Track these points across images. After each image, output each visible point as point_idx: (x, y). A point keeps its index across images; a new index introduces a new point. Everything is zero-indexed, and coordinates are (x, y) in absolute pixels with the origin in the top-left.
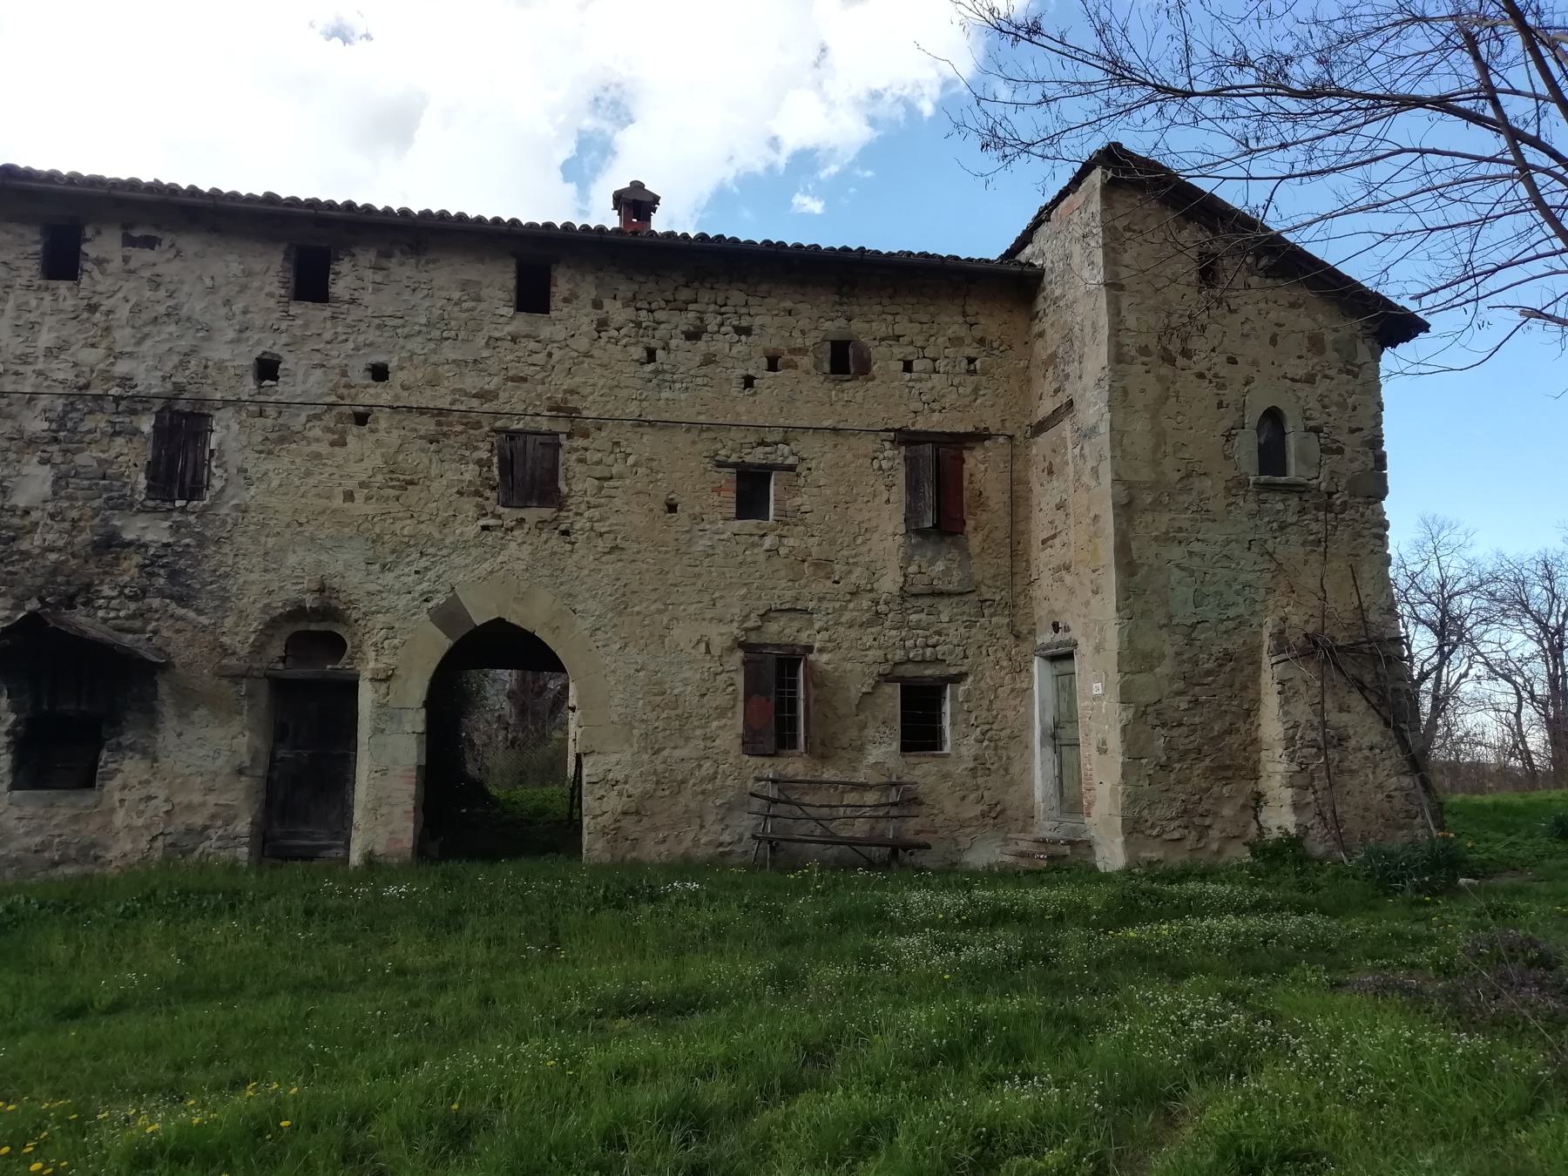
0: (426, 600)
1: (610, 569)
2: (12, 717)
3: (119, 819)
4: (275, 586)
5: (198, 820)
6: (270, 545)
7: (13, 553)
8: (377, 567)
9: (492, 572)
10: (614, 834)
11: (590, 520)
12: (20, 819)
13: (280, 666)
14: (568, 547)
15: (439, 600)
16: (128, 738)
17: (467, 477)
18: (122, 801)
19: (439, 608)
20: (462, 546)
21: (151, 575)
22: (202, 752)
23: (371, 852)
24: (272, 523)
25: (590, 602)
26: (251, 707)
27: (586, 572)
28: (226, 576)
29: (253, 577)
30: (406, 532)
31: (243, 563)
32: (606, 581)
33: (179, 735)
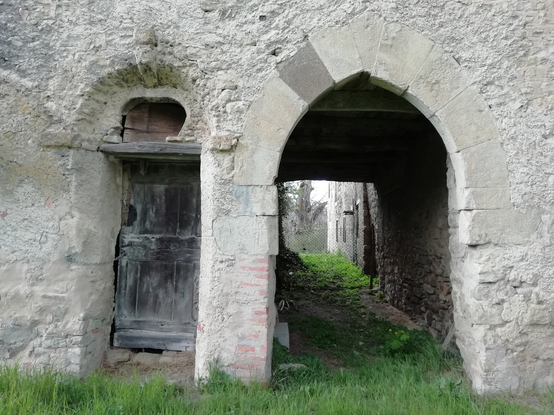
0: (274, 53)
4: (101, 40)
5: (27, 314)
8: (215, 15)
9: (352, 14)
10: (520, 351)
13: (116, 138)
15: (288, 51)
23: (217, 361)
26: (79, 185)
27: (472, 9)
28: (49, 30)
29: (79, 30)
31: (66, 15)
32: (498, 19)
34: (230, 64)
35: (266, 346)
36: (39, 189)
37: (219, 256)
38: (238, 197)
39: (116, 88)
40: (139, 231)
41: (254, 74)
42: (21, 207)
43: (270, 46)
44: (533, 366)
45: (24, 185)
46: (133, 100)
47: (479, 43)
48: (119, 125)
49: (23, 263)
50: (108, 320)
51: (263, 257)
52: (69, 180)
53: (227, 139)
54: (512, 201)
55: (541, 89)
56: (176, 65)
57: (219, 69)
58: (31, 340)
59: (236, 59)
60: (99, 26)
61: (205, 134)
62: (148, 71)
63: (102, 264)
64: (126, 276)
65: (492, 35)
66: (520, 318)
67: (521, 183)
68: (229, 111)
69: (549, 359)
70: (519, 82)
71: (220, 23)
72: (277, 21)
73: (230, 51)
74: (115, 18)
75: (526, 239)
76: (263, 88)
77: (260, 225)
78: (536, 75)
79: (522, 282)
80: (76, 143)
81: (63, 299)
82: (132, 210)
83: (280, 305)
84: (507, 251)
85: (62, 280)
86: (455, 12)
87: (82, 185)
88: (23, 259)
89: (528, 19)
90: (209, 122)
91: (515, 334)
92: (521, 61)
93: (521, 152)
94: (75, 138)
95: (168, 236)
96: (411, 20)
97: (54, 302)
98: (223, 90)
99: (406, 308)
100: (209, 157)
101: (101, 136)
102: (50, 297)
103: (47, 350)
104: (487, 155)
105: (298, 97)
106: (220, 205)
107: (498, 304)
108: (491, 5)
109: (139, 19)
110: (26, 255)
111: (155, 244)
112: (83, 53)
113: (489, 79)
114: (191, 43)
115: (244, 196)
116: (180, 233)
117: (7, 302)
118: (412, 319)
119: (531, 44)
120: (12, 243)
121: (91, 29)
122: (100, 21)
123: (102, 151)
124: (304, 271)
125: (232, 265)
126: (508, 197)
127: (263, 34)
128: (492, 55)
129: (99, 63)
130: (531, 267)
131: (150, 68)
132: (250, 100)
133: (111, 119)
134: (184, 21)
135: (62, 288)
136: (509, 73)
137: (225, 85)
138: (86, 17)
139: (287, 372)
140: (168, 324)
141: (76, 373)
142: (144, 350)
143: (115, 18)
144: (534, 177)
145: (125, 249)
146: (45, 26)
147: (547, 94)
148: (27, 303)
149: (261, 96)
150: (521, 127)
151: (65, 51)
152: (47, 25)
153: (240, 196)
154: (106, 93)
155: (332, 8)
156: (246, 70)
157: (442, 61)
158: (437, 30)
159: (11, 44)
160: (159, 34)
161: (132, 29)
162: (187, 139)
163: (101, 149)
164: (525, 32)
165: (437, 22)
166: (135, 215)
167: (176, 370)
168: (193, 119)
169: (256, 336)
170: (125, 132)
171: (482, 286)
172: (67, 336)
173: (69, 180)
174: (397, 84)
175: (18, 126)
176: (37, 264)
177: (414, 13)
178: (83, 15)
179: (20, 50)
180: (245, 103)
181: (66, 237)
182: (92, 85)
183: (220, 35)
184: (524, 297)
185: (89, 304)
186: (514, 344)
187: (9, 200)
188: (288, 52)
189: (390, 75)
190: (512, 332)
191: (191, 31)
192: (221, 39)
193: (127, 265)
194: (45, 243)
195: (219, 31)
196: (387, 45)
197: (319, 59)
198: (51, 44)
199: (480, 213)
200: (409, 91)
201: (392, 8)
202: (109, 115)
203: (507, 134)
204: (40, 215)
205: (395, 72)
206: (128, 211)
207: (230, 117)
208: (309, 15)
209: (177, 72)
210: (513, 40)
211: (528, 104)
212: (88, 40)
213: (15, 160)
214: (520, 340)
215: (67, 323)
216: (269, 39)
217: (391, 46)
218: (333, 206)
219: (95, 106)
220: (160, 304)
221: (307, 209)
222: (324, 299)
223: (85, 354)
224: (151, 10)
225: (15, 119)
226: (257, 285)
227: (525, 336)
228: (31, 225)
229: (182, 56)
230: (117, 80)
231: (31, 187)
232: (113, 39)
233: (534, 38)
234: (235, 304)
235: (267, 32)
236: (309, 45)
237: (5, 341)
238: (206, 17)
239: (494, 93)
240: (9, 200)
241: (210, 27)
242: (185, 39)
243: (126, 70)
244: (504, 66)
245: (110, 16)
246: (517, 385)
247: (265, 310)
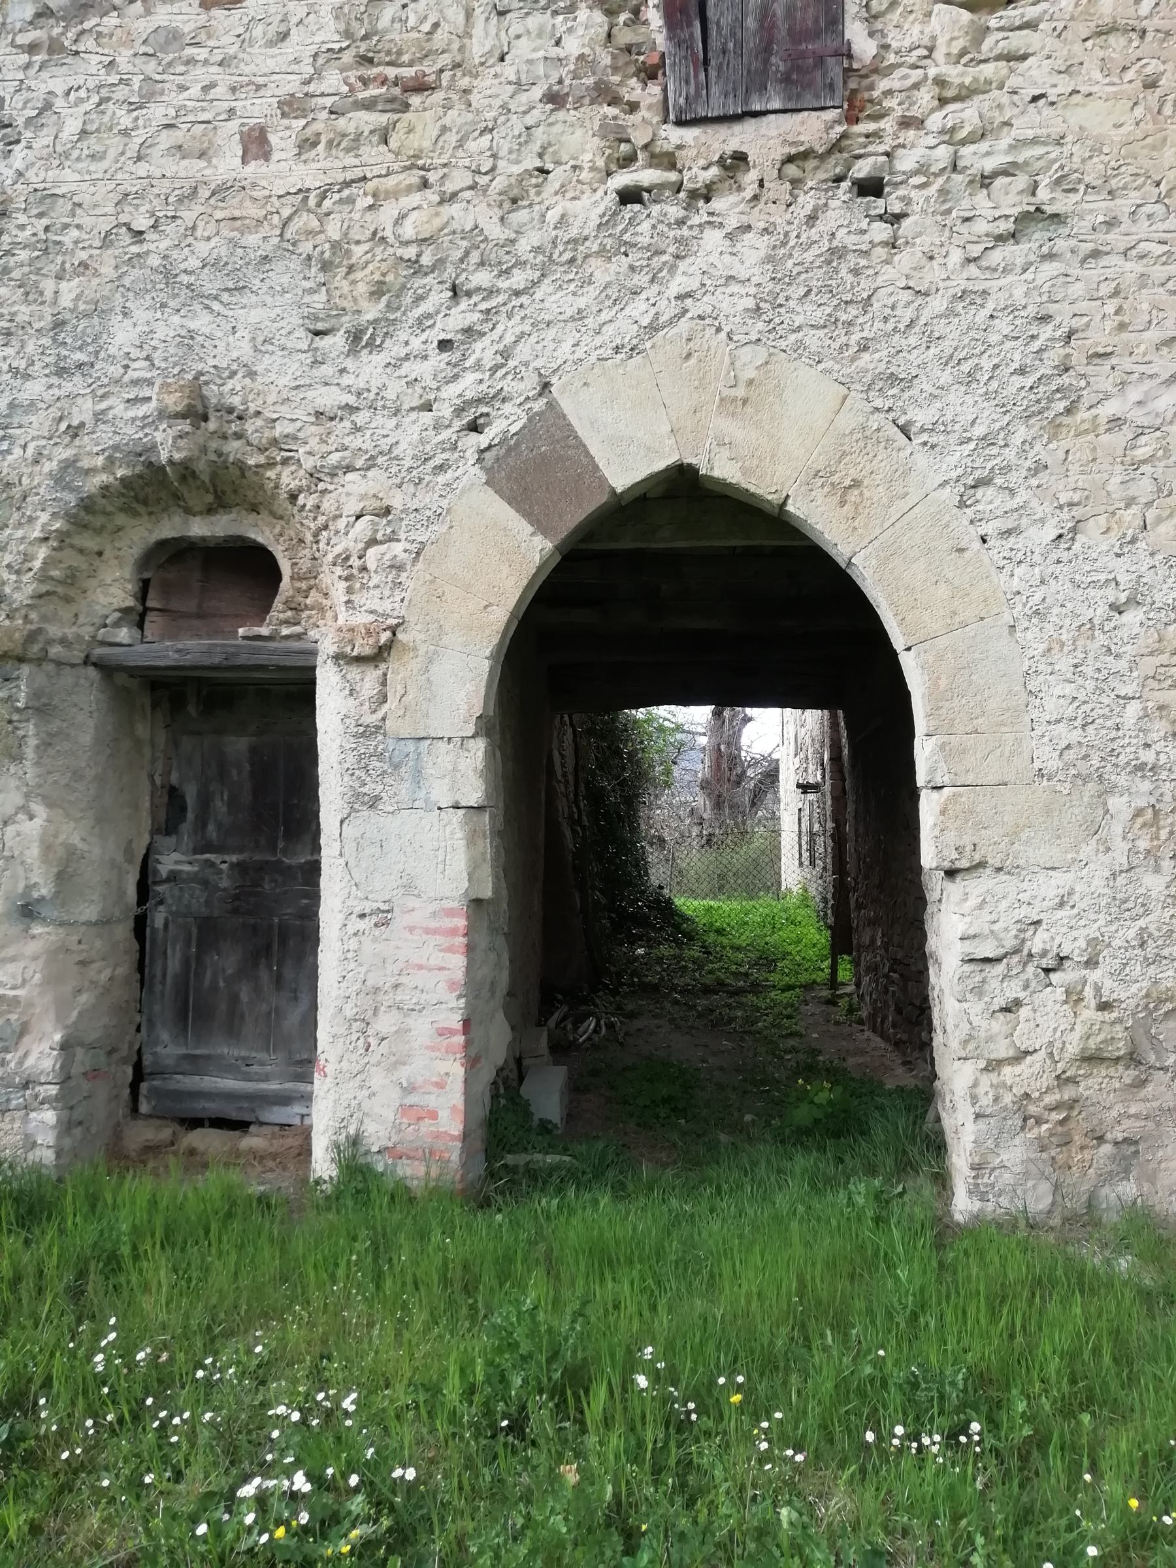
0: (474, 427)
1: (1016, 288)
4: (82, 412)
6: (66, 301)
8: (337, 342)
9: (653, 328)
10: (1059, 1123)
11: (949, 134)
13: (124, 634)
14: (881, 232)
15: (506, 422)
17: (573, 47)
19: (509, 446)
20: (565, 257)
23: (355, 1141)
25: (955, 396)
26: (45, 745)
27: (938, 304)
29: (34, 389)
30: (408, 230)
32: (1003, 326)
34: (372, 458)
35: (461, 1107)
37: (356, 903)
38: (396, 767)
39: (121, 519)
40: (191, 846)
41: (427, 478)
43: (463, 410)
44: (1087, 1156)
46: (162, 544)
47: (956, 387)
48: (130, 602)
50: (124, 1051)
51: (456, 905)
52: (21, 733)
53: (369, 633)
54: (1037, 765)
55: (1108, 493)
56: (251, 462)
57: (349, 469)
59: (385, 444)
60: (77, 379)
61: (328, 619)
62: (190, 480)
63: (104, 922)
64: (165, 953)
65: (987, 364)
66: (1058, 1044)
67: (1058, 721)
68: (372, 566)
69: (1127, 1141)
70: (1053, 478)
71: (349, 360)
72: (478, 351)
73: (373, 425)
74: (111, 359)
75: (1069, 856)
76: (448, 510)
77: (448, 830)
78: (1094, 460)
79: (1062, 959)
80: (36, 648)
81: (16, 1001)
82: (174, 795)
83: (581, 1030)
84: (1025, 885)
85: (13, 959)
86: (897, 313)
87: (50, 744)
89: (1077, 323)
90: (333, 592)
91: (1047, 1080)
92: (1059, 425)
93: (1057, 647)
94: (32, 637)
95: (257, 857)
96: (793, 337)
98: (358, 517)
99: (895, 1034)
100: (331, 674)
101: (91, 629)
104: (977, 656)
105: (531, 529)
106: (356, 784)
107: (1006, 1010)
108: (985, 293)
109: (166, 360)
111: (229, 877)
112: (44, 442)
113: (979, 472)
114: (284, 410)
115: (411, 763)
116: (285, 851)
118: (905, 1063)
119: (1083, 383)
122: (80, 366)
123: (95, 665)
124: (679, 945)
125: (386, 923)
126: (1026, 756)
127: (447, 383)
128: (987, 413)
129: (79, 464)
130: (1083, 922)
131: (194, 472)
132: (420, 539)
133: (112, 590)
134: (267, 359)
135: (14, 976)
136: (1030, 455)
137: (361, 505)
138: (48, 360)
139: (521, 1170)
140: (262, 1064)
141: (46, 1166)
142: (207, 1123)
143: (111, 359)
144: (1090, 706)
145: (160, 888)
147: (1122, 505)
149: (444, 528)
150: (1059, 588)
153: (401, 762)
154: (99, 531)
155: (605, 316)
156: (410, 470)
157: (868, 433)
158: (853, 360)
160: (212, 391)
161: (150, 383)
162: (285, 631)
163: (93, 659)
164: (1068, 356)
165: (854, 338)
166: (183, 809)
167: (271, 1164)
168: (298, 584)
169: (440, 1085)
170: (148, 619)
171: (968, 968)
172: (26, 1085)
173: (21, 733)
174: (760, 492)
177: (799, 320)
180: (408, 546)
182: (67, 514)
183: (348, 389)
184: (1068, 993)
185: (75, 1013)
186: (1042, 1104)
188: (506, 423)
189: (744, 471)
190: (1038, 1076)
191: (284, 381)
192: (351, 400)
193: (166, 926)
195: (347, 380)
196: (735, 400)
197: (576, 437)
199: (961, 795)
200: (790, 508)
201: (747, 310)
202: (109, 581)
203: (1024, 605)
205: (755, 463)
206: (166, 799)
207: (375, 580)
208: (551, 333)
209: (255, 478)
210: (1038, 375)
211: (1074, 530)
212: (54, 412)
214: (1058, 1097)
215: (26, 1055)
216: (460, 395)
217: (745, 401)
218: (792, 770)
219: (77, 561)
220: (242, 1017)
221: (733, 778)
222: (700, 1016)
223: (66, 1127)
224: (192, 338)
226: (441, 969)
227: (1071, 1086)
229: (264, 441)
230: (123, 500)
232: (111, 408)
233: (1091, 367)
234: (394, 1011)
235: (456, 377)
236: (552, 405)
238: (316, 349)
239: (991, 507)
241: (327, 370)
242: (270, 400)
243: (140, 476)
244: (1017, 440)
245: (102, 355)
246: (1049, 1200)
247: (459, 1026)
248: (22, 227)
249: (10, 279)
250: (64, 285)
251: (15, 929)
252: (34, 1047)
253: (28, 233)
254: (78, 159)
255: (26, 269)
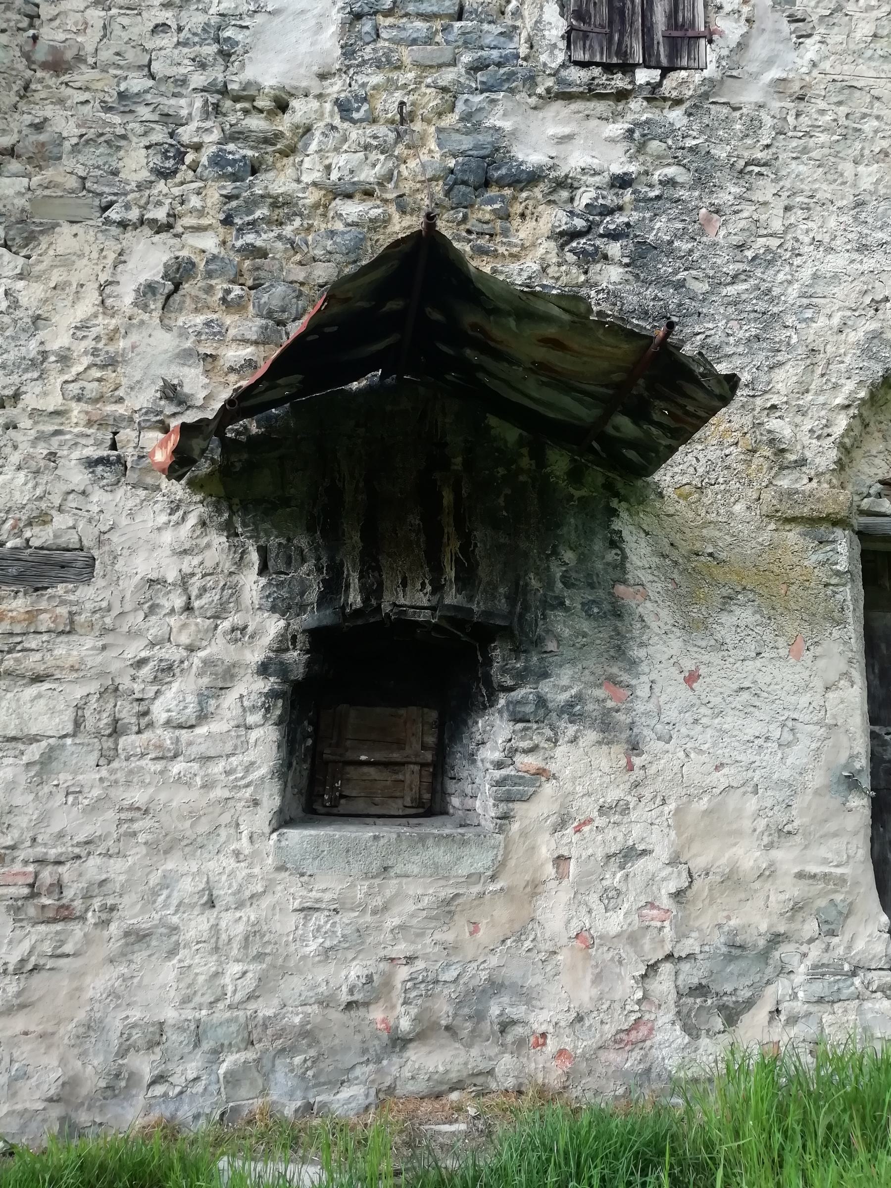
2: (274, 626)
3: (556, 914)
5: (756, 919)
7: (253, 203)
12: (307, 910)
16: (561, 686)
18: (561, 860)
21: (588, 258)
22: (753, 728)
24: (868, 126)
28: (769, 260)
29: (837, 262)
31: (805, 230)
33: (692, 678)
36: (769, 618)
42: (732, 660)
45: (734, 608)
49: (744, 793)
58: (769, 983)
85: (835, 835)
88: (743, 785)
97: (824, 888)
102: (814, 877)
103: (814, 1008)
110: (750, 774)
112: (849, 313)
117: (710, 890)
120: (714, 745)
121: (861, 262)
133: (877, 461)
138: (850, 236)
146: (762, 251)
148: (756, 891)
151: (808, 306)
152: (768, 249)
159: (684, 286)
175: (708, 472)
176: (777, 794)
178: (845, 230)
179: (704, 300)
181: (842, 730)
187: (703, 644)
194: (789, 745)
198: (776, 291)
202: (874, 452)
204: (778, 679)
212: (859, 286)
213: (710, 551)
225: (700, 456)
228: (757, 704)
231: (749, 611)
237: (714, 988)
240: (703, 644)
248: (822, 112)
249: (810, 159)
250: (861, 169)
251: (834, 802)
252: (861, 929)
253: (828, 118)
254: (870, 58)
255: (826, 151)
